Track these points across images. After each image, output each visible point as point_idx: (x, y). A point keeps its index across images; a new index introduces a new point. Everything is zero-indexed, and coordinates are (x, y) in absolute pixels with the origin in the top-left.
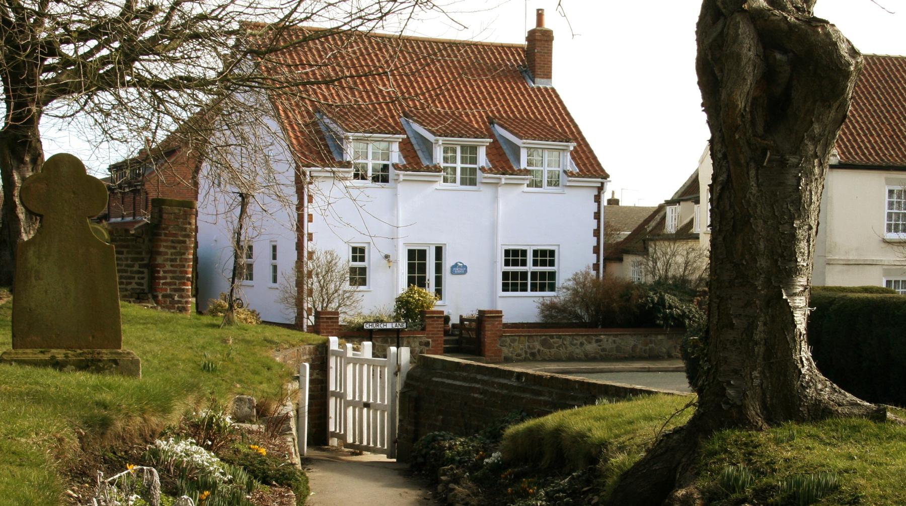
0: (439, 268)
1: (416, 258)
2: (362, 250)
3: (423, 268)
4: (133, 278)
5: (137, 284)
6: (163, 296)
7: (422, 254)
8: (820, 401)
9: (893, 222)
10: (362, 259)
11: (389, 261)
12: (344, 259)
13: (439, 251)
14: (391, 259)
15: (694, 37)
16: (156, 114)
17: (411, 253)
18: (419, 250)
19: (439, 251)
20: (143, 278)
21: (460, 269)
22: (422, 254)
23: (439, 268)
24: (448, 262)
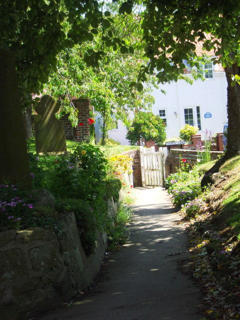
0: (198, 116)
1: (188, 113)
2: (164, 111)
3: (191, 116)
4: (67, 131)
5: (69, 133)
6: (79, 137)
7: (191, 110)
8: (145, 13)
9: (188, 114)
10: (164, 115)
11: (176, 115)
12: (157, 113)
13: (198, 108)
14: (177, 113)
15: (226, 108)
16: (120, 24)
17: (186, 111)
18: (189, 109)
19: (198, 108)
20: (71, 131)
21: (208, 115)
22: (191, 110)
23: (198, 116)
24: (202, 114)
